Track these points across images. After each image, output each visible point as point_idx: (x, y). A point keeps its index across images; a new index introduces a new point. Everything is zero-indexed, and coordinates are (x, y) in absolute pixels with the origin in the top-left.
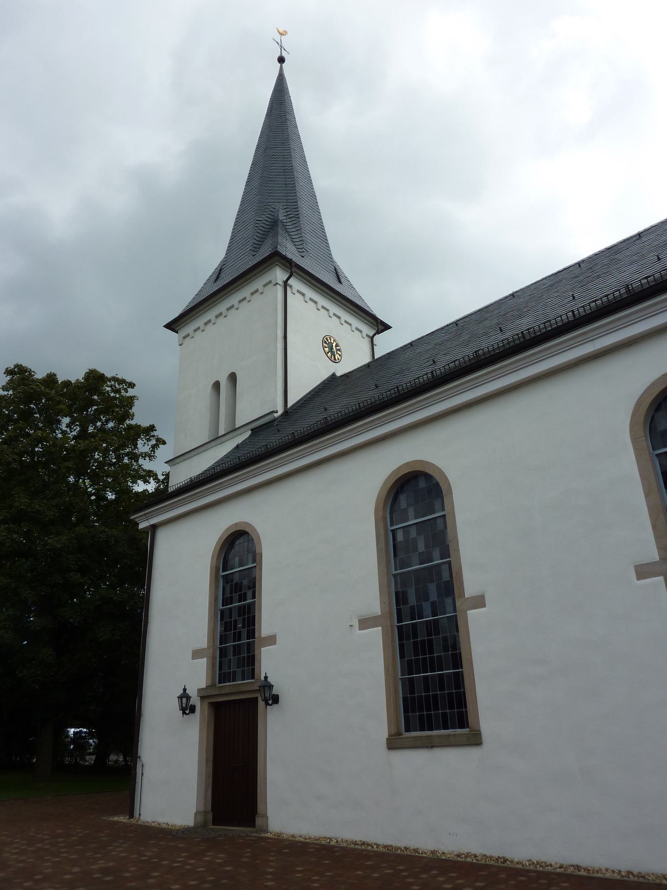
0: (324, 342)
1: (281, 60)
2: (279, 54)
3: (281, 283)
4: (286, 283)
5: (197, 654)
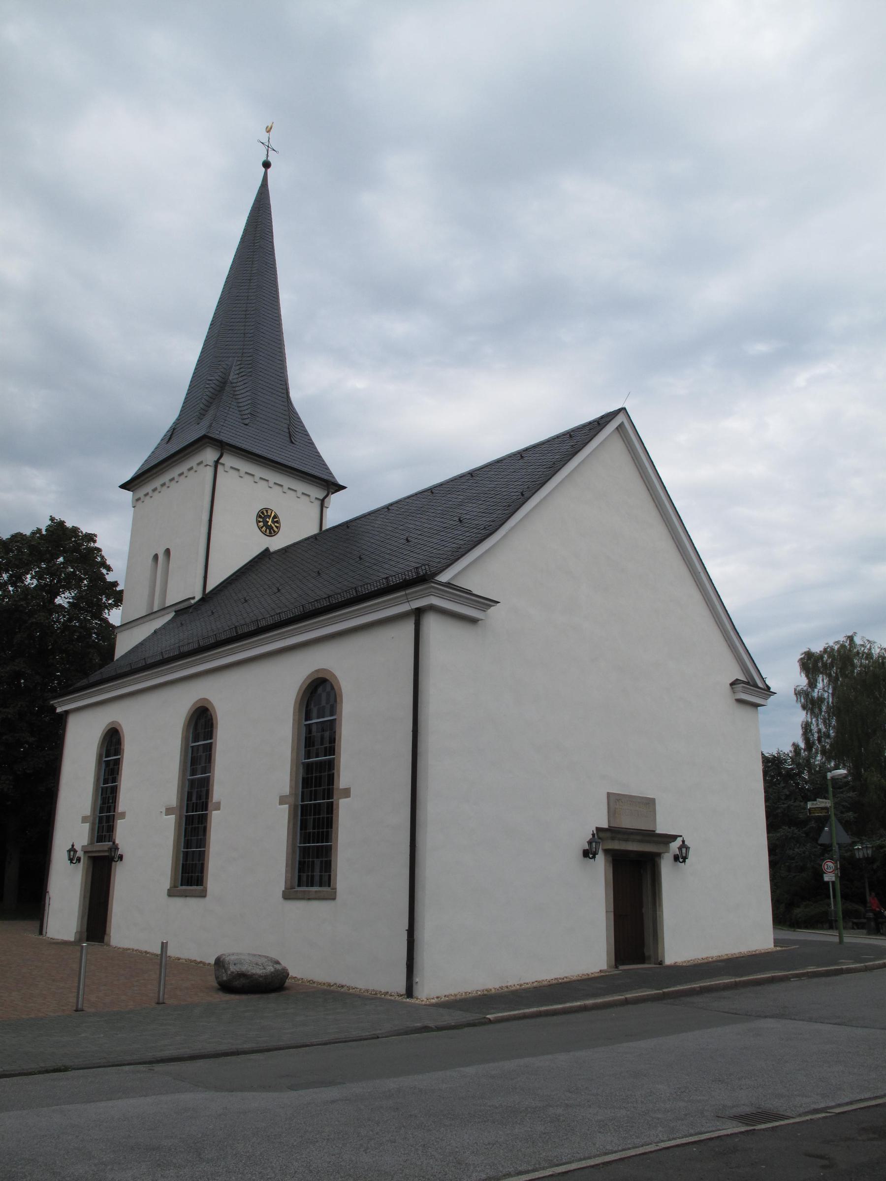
0: (259, 516)
1: (267, 165)
2: (264, 158)
3: (212, 463)
4: (217, 463)
5: (169, 811)
